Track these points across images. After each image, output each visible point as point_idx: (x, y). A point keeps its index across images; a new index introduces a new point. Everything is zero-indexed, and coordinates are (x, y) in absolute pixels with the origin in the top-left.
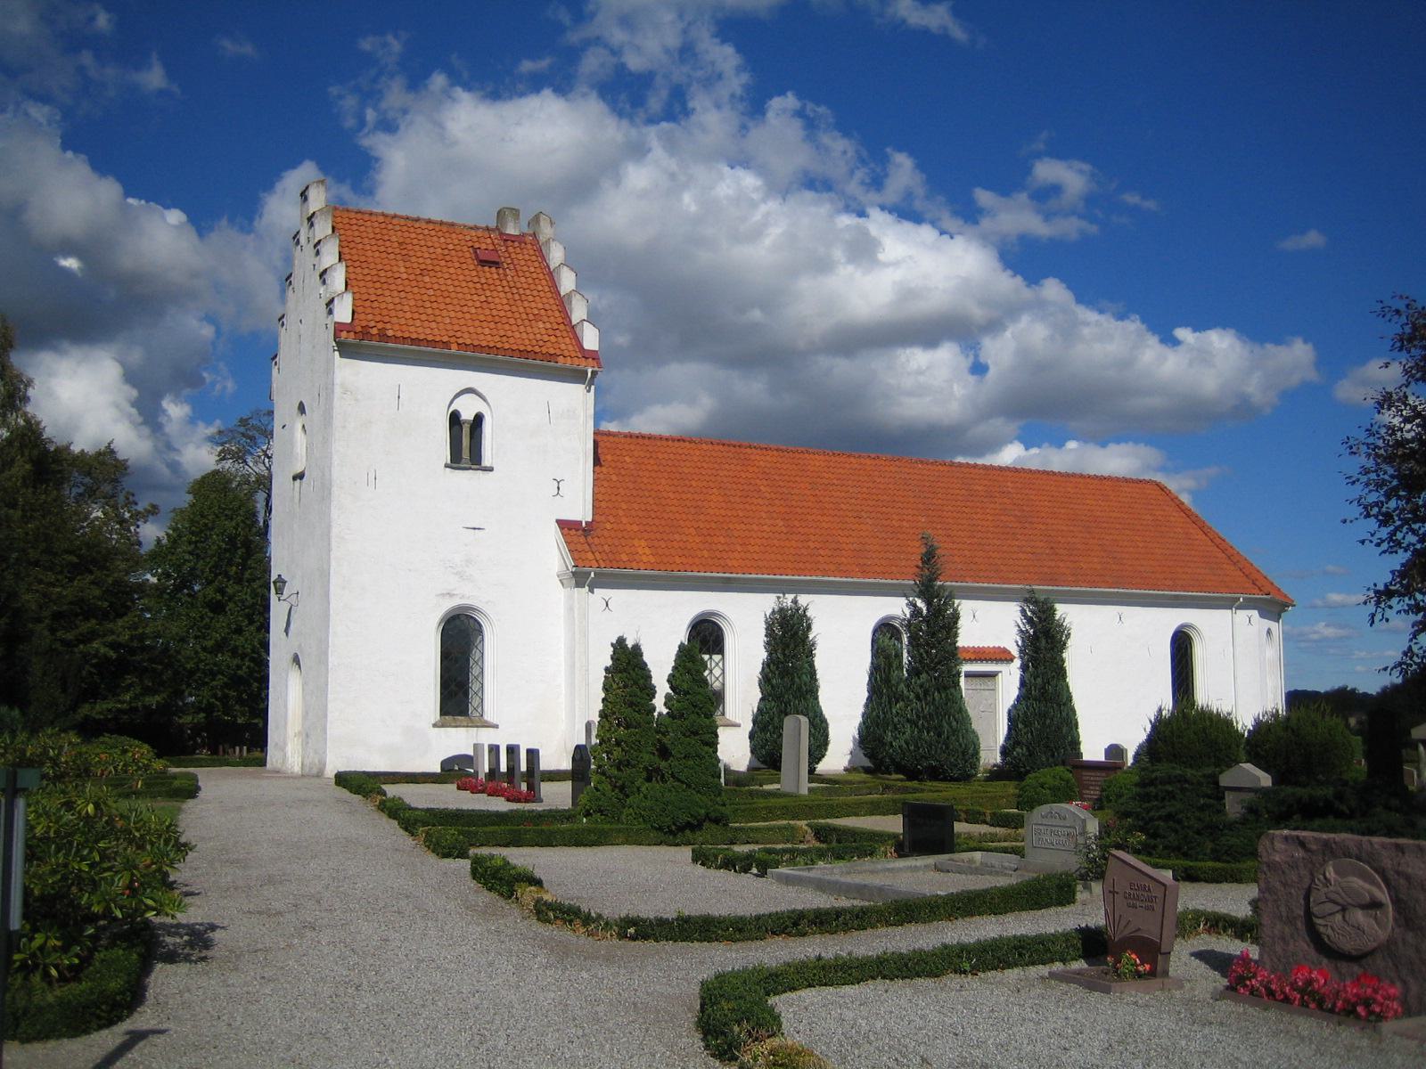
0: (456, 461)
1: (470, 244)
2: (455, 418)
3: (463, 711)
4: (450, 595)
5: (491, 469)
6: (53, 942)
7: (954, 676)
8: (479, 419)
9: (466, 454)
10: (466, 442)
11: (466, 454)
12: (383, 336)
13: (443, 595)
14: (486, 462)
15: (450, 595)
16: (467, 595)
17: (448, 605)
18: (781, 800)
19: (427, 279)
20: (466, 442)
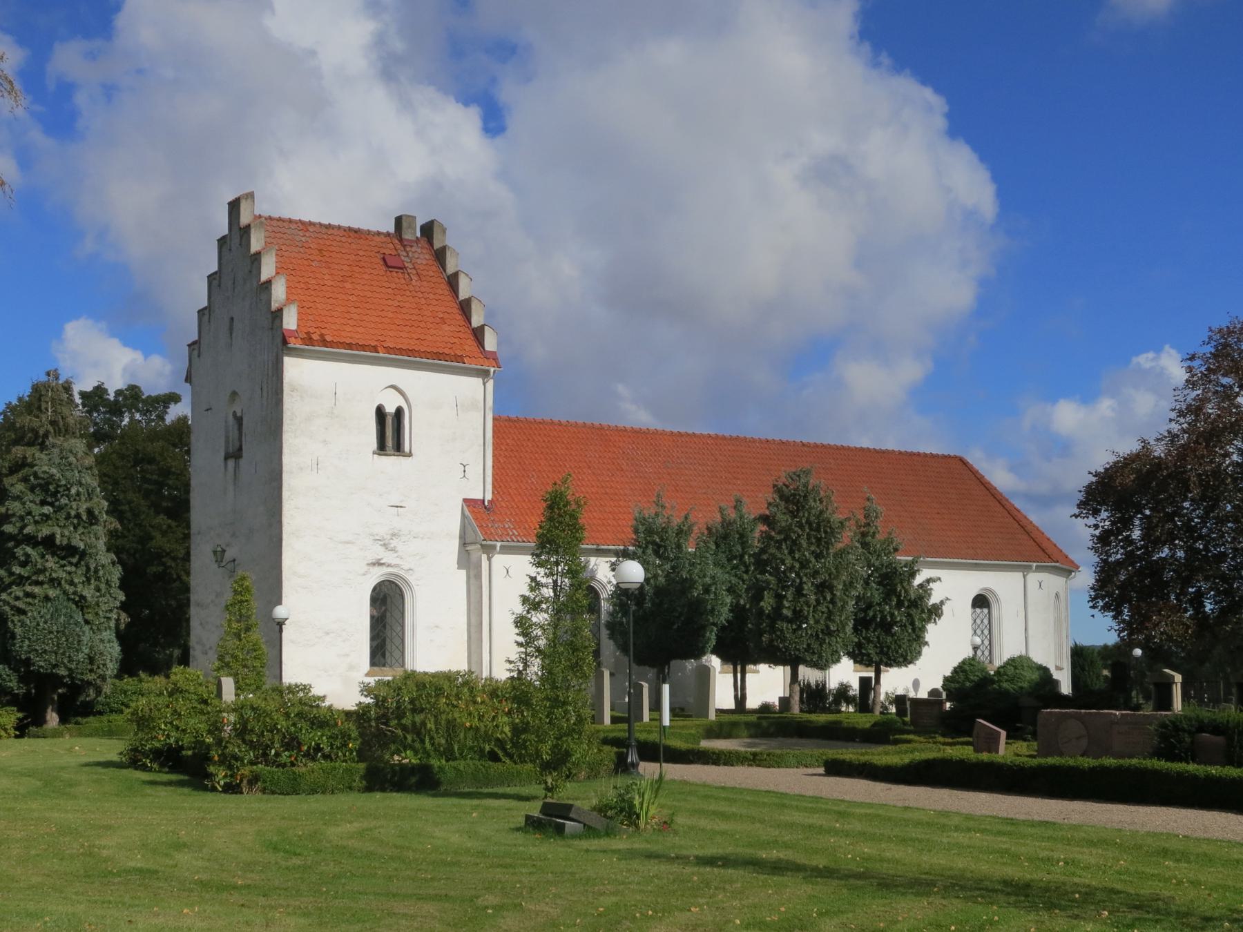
0: (382, 447)
1: (376, 249)
2: (380, 413)
3: (398, 448)
4: (378, 563)
5: (410, 455)
6: (225, 715)
7: (901, 712)
8: (399, 411)
9: (390, 443)
10: (390, 432)
11: (390, 443)
12: (324, 343)
13: (374, 564)
14: (407, 449)
15: (378, 563)
16: (390, 462)
17: (376, 576)
18: (712, 808)
19: (348, 285)
20: (390, 432)
